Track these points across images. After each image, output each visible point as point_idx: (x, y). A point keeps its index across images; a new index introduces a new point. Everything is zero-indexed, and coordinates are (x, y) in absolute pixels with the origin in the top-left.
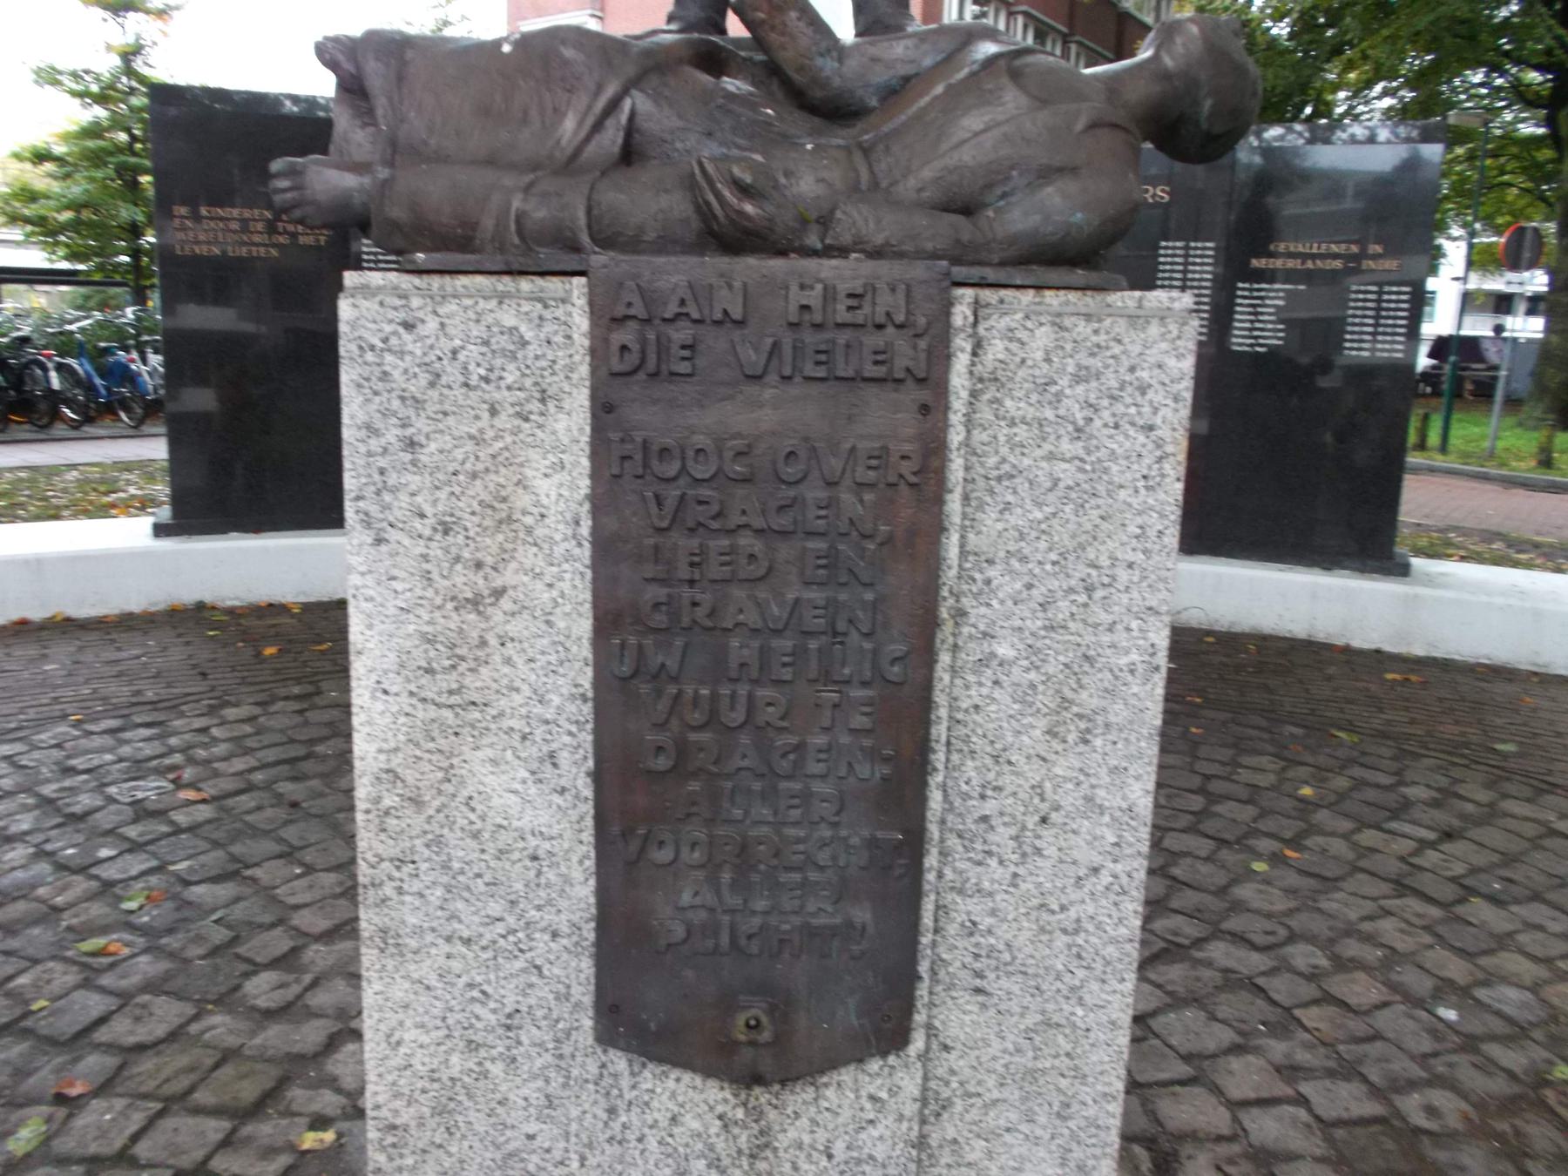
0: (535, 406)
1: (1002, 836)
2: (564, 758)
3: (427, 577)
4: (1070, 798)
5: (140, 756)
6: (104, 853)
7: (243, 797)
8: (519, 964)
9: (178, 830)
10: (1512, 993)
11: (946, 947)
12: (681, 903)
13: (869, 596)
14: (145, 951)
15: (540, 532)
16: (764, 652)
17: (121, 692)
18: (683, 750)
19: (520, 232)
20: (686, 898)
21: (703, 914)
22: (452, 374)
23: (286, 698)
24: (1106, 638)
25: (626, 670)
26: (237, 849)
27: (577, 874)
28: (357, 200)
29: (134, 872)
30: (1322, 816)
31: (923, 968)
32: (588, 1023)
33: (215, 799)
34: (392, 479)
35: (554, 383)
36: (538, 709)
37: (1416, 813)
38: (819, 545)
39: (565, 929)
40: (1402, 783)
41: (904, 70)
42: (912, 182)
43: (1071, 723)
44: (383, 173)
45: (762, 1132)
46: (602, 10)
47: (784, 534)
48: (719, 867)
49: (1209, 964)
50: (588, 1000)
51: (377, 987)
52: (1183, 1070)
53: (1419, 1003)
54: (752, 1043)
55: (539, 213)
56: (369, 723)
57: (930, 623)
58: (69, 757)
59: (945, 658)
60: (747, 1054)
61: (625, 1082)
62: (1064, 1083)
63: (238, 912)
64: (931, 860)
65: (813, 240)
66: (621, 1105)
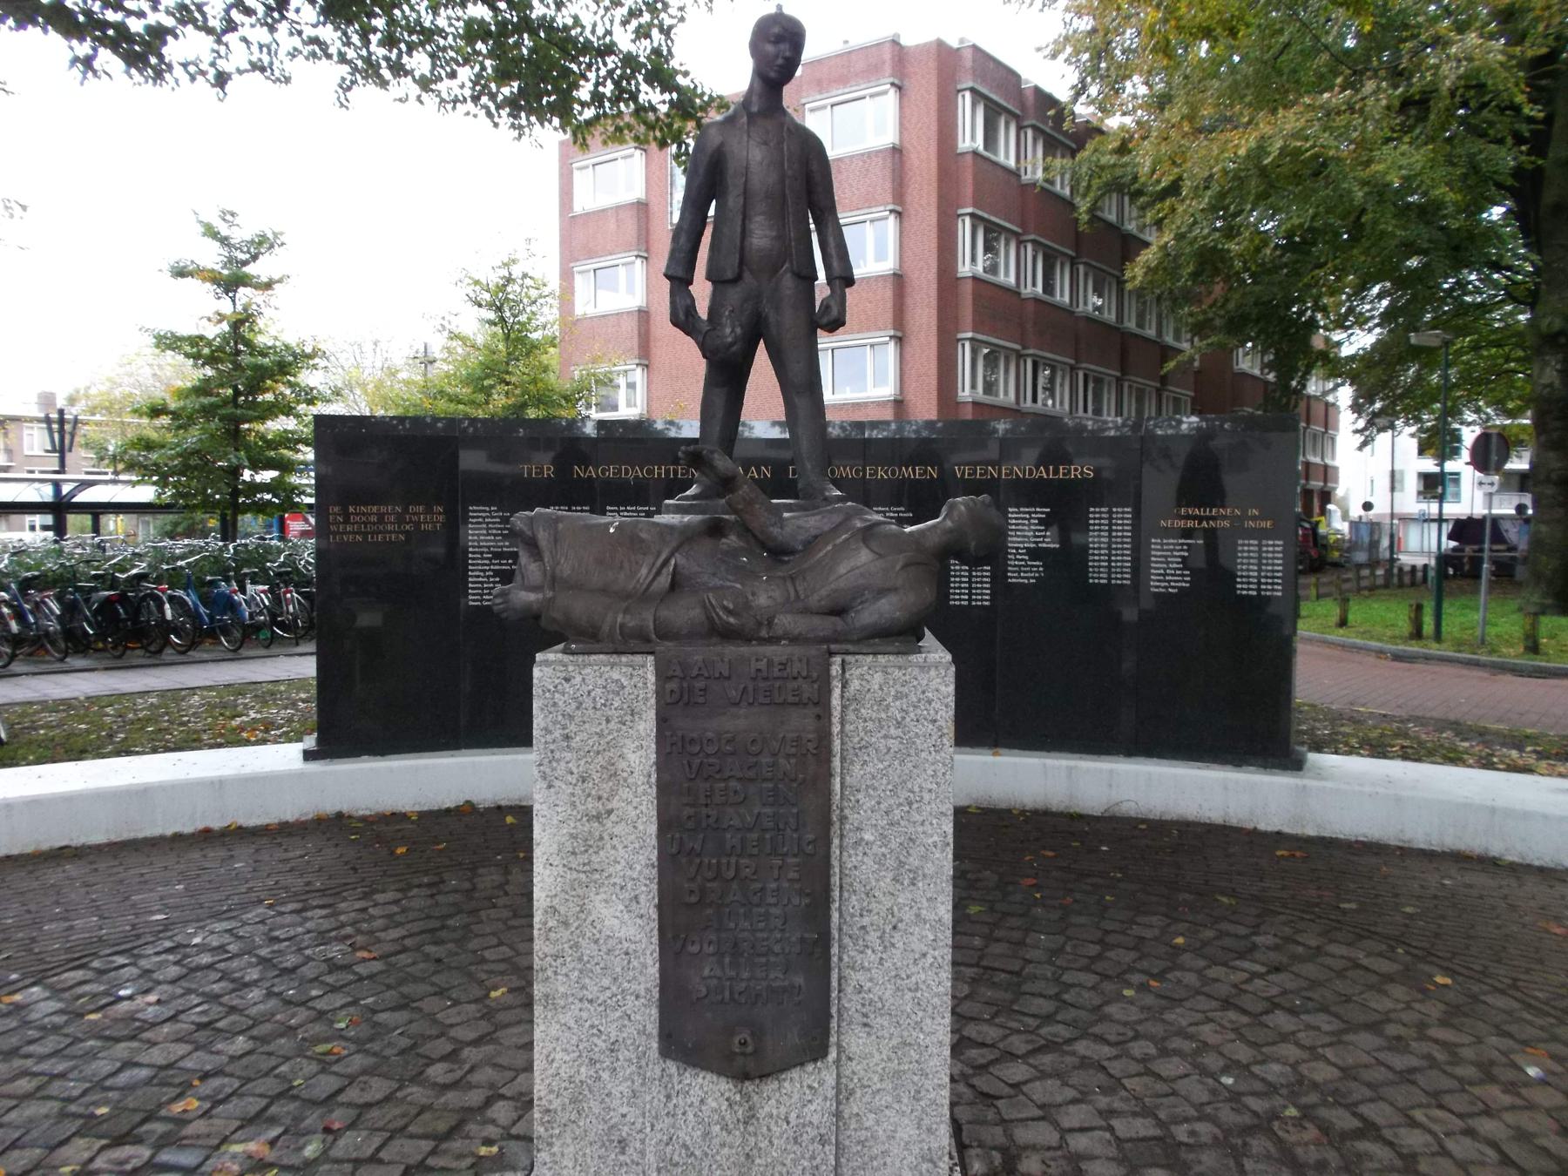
0: (628, 718)
1: (873, 937)
2: (642, 898)
3: (573, 804)
4: (908, 916)
5: (323, 928)
6: (314, 993)
7: (402, 956)
8: (618, 1014)
9: (361, 979)
10: (1276, 1067)
11: (847, 1002)
12: (705, 974)
13: (795, 810)
14: (358, 1052)
15: (630, 780)
16: (743, 840)
17: (298, 883)
18: (703, 891)
19: (621, 634)
20: (706, 972)
21: (715, 981)
22: (588, 703)
23: (419, 886)
24: (920, 829)
25: (674, 850)
26: (405, 989)
27: (650, 962)
28: (535, 606)
29: (338, 1005)
30: (1186, 958)
31: (834, 1011)
32: (655, 1045)
33: (381, 958)
34: (557, 755)
35: (639, 706)
36: (629, 873)
37: (1257, 955)
38: (771, 785)
39: (643, 993)
40: (1255, 934)
41: (814, 532)
42: (816, 597)
43: (905, 875)
44: (549, 594)
45: (750, 1109)
46: (647, 250)
47: (751, 780)
48: (723, 955)
49: (1073, 1053)
50: (655, 1032)
51: (542, 1028)
52: (1038, 1113)
53: (1213, 1076)
54: (743, 1054)
55: (632, 623)
56: (542, 881)
57: (828, 823)
58: (271, 930)
59: (836, 841)
60: (740, 1061)
61: (675, 1080)
62: (916, 1078)
63: (414, 1028)
64: (835, 950)
65: (764, 633)
66: (674, 1094)
